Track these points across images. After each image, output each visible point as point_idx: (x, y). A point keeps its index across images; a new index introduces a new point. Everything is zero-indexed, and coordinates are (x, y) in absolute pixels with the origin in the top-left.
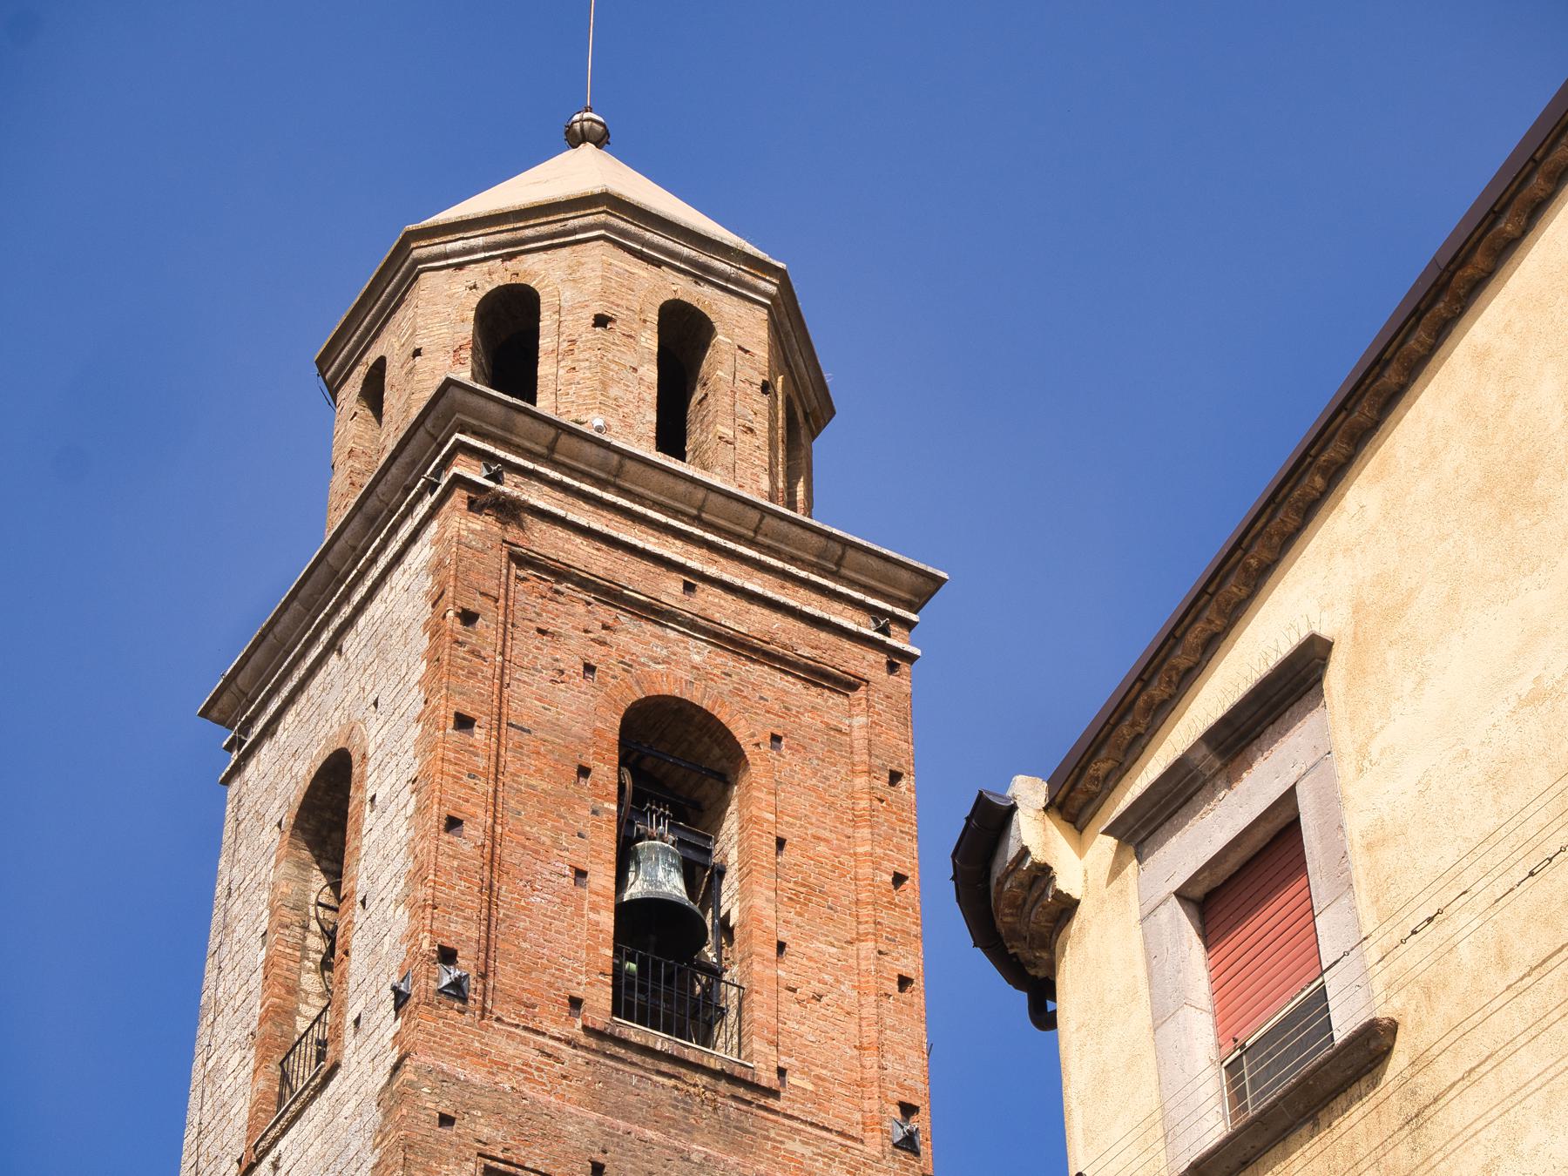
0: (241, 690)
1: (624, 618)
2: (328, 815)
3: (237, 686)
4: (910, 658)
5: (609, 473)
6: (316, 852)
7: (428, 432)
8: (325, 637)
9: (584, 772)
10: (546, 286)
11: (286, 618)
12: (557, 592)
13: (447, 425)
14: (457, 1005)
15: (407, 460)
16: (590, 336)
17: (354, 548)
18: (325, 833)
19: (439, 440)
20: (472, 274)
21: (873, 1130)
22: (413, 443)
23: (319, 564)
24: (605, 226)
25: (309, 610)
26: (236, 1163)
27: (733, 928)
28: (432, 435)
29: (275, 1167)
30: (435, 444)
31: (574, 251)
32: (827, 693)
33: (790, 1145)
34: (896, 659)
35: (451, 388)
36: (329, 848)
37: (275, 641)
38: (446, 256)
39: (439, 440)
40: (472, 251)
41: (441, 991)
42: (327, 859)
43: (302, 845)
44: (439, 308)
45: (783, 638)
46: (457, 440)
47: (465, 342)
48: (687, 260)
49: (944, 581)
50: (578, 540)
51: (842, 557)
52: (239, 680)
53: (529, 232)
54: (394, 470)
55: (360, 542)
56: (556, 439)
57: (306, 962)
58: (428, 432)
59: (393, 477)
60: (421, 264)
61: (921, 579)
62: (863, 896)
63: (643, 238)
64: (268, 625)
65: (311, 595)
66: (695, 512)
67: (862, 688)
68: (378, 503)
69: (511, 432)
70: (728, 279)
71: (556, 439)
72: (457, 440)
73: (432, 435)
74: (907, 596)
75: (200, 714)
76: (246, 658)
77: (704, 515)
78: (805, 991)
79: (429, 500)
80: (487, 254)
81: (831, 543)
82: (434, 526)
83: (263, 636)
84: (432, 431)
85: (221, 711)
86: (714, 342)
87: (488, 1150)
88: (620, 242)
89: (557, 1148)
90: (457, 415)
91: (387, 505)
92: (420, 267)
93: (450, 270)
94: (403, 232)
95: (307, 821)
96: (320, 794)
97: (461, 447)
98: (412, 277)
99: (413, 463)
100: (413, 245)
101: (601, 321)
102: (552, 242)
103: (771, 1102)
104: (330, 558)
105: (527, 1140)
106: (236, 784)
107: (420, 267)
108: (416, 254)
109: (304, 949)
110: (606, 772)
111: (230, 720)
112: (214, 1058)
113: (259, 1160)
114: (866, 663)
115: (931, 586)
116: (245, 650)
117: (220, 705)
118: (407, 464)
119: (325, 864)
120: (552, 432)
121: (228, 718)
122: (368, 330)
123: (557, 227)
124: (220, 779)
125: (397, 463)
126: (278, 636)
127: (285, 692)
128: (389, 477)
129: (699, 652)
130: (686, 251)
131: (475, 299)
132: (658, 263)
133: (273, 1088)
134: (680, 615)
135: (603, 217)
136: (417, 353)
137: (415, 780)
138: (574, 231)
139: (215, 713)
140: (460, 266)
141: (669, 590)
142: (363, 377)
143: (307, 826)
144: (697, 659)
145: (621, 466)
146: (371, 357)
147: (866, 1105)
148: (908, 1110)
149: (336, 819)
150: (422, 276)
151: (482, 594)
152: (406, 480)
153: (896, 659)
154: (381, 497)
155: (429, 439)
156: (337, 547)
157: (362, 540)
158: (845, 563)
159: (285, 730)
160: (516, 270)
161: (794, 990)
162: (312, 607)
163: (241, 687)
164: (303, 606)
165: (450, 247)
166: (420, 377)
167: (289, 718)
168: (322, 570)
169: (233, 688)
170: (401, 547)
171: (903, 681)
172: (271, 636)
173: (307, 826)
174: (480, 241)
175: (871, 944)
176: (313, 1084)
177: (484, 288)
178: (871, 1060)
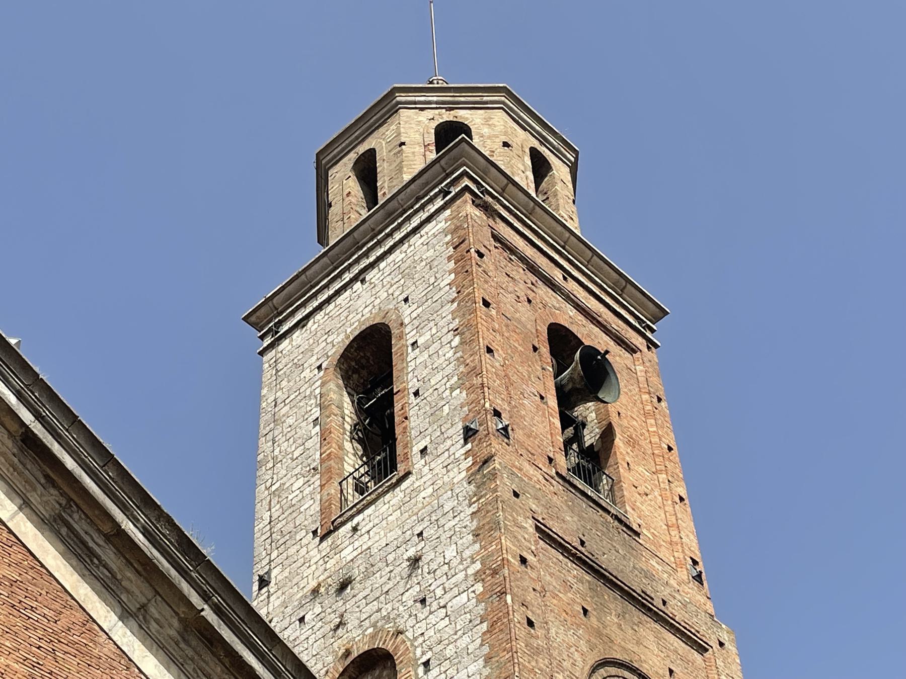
0: (274, 306)
1: (540, 282)
2: (353, 364)
3: (273, 303)
4: (656, 346)
5: (527, 211)
6: (346, 383)
7: (442, 167)
8: (356, 270)
9: (535, 349)
10: (474, 124)
11: (317, 267)
12: (510, 259)
13: (455, 163)
14: (506, 440)
15: (423, 182)
16: (502, 150)
17: (373, 230)
18: (350, 373)
19: (447, 172)
20: (430, 113)
21: (682, 568)
22: (430, 172)
23: (347, 237)
24: (503, 103)
25: (333, 263)
26: (311, 534)
27: (598, 452)
28: (443, 169)
29: (355, 529)
30: (444, 174)
31: (486, 112)
32: (624, 350)
33: (651, 562)
34: (651, 344)
35: (464, 143)
36: (351, 382)
37: (306, 279)
38: (415, 103)
39: (447, 172)
40: (430, 103)
41: (498, 430)
42: (350, 387)
43: (340, 377)
44: (413, 126)
45: (605, 317)
46: (465, 170)
47: (431, 142)
48: (537, 132)
49: (668, 313)
50: (518, 237)
51: (625, 287)
52: (275, 301)
53: (462, 99)
54: (412, 186)
55: (378, 226)
56: (507, 185)
57: (345, 436)
58: (442, 167)
59: (411, 190)
60: (401, 104)
61: (658, 310)
62: (656, 452)
63: (519, 115)
64: (303, 270)
65: (337, 255)
66: (563, 244)
67: (638, 353)
68: (397, 205)
69: (486, 175)
70: (554, 147)
71: (507, 185)
72: (465, 170)
73: (443, 169)
74: (651, 317)
75: (243, 319)
76: (283, 288)
77: (567, 247)
78: (641, 489)
79: (439, 203)
80: (438, 106)
81: (621, 279)
82: (448, 212)
83: (297, 277)
84: (445, 166)
85: (258, 318)
86: (551, 174)
87: (536, 516)
88: (508, 112)
89: (565, 526)
90: (464, 159)
91: (402, 206)
92: (400, 106)
93: (417, 110)
94: (392, 87)
95: (343, 364)
96: (352, 350)
97: (465, 174)
98: (394, 111)
99: (427, 184)
100: (397, 95)
101: (506, 144)
102: (474, 106)
103: (637, 538)
104: (355, 234)
105: (551, 517)
106: (271, 354)
107: (400, 106)
108: (398, 99)
109: (344, 429)
110: (545, 350)
111: (262, 323)
112: (277, 485)
113: (343, 523)
114: (638, 341)
115: (661, 315)
116: (283, 284)
117: (258, 314)
118: (423, 184)
119: (349, 389)
120: (506, 181)
121: (261, 322)
122: (357, 138)
123: (478, 99)
124: (258, 351)
125: (416, 183)
126: (308, 277)
127: (315, 304)
128: (408, 190)
129: (572, 312)
130: (537, 128)
131: (434, 124)
132: (525, 129)
133: (337, 495)
134: (563, 290)
135: (503, 98)
136: (403, 144)
137: (457, 330)
138: (486, 103)
139: (253, 319)
140: (422, 109)
141: (558, 275)
142: (353, 161)
143: (342, 367)
144: (571, 314)
145: (534, 208)
146: (362, 149)
147: (676, 554)
148: (695, 563)
149: (357, 367)
150: (401, 110)
151: (484, 246)
152: (419, 192)
153: (651, 344)
154: (400, 201)
155: (441, 170)
156: (361, 228)
157: (379, 225)
158: (625, 291)
159: (314, 323)
160: (456, 115)
161: (636, 488)
162: (335, 262)
163: (275, 305)
164: (330, 260)
165: (417, 99)
166: (406, 155)
167: (319, 317)
168: (349, 240)
169: (270, 303)
170: (419, 224)
171: (652, 355)
172: (303, 277)
173: (342, 367)
174: (435, 99)
175: (664, 476)
176: (387, 485)
177: (438, 120)
178: (674, 533)
